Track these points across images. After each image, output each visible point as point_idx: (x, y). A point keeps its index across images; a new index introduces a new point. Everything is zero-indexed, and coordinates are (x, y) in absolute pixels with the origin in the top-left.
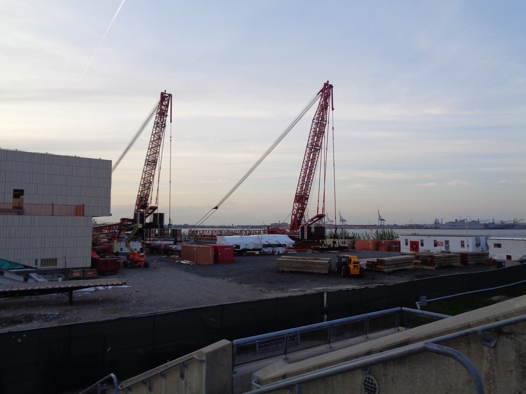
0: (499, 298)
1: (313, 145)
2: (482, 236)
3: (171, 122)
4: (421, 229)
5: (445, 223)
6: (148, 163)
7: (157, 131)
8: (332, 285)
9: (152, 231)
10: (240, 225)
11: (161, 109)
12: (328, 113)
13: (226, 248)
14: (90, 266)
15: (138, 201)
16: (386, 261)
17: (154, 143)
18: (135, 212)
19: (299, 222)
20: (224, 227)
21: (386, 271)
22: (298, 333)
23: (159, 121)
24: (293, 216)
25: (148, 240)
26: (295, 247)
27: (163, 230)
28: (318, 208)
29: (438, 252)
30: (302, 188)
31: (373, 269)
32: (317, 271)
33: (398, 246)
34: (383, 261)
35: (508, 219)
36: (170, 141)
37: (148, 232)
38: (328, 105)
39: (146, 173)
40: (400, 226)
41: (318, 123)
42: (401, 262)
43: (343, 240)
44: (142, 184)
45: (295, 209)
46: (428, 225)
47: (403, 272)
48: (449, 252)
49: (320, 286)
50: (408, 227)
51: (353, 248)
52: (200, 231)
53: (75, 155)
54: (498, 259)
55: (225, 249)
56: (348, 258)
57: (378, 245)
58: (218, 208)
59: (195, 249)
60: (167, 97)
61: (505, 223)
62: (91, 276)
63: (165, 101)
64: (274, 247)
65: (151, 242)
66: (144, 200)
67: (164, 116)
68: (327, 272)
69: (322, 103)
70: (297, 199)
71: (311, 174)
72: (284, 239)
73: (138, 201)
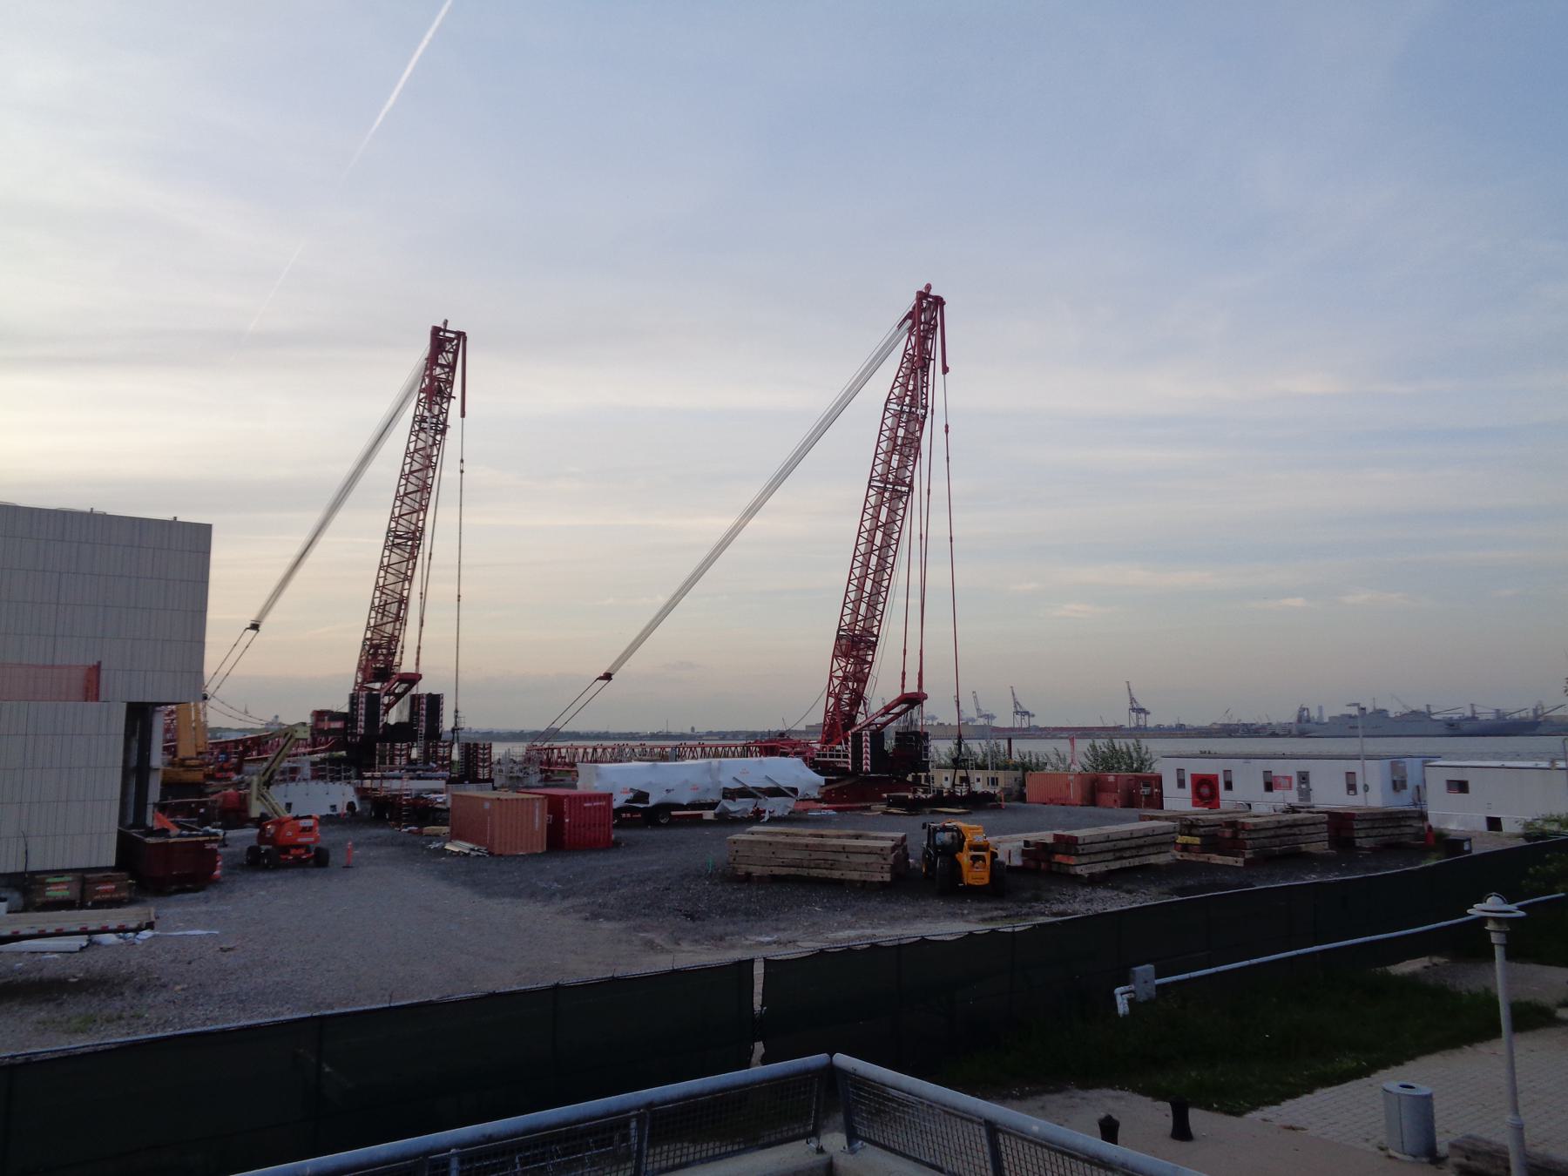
0: (1426, 964)
1: (886, 482)
2: (1411, 757)
3: (463, 415)
4: (1257, 737)
5: (1330, 718)
6: (393, 541)
7: (421, 444)
8: (893, 920)
9: (398, 750)
10: (715, 730)
11: (433, 378)
12: (931, 382)
13: (590, 802)
14: (112, 862)
15: (364, 658)
16: (1080, 842)
17: (412, 479)
18: (355, 690)
19: (851, 719)
20: (668, 736)
21: (1082, 873)
22: (632, 1113)
23: (426, 414)
24: (832, 700)
25: (368, 778)
26: (826, 798)
27: (433, 747)
28: (904, 674)
29: (1277, 809)
30: (856, 611)
31: (1043, 865)
32: (855, 876)
33: (1156, 790)
34: (1073, 841)
35: (1518, 705)
36: (459, 474)
37: (387, 753)
38: (930, 359)
39: (390, 570)
40: (1195, 729)
41: (902, 412)
42: (1133, 843)
43: (990, 773)
44: (376, 604)
45: (837, 677)
46: (1280, 724)
47: (1139, 876)
48: (1309, 811)
49: (850, 927)
50: (1217, 733)
51: (1022, 797)
52: (560, 749)
53: (92, 509)
54: (1461, 829)
55: (586, 805)
56: (959, 831)
57: (1093, 791)
58: (613, 677)
59: (487, 805)
60: (451, 340)
61: (1508, 718)
62: (108, 896)
63: (444, 354)
64: (760, 798)
65: (376, 784)
66: (382, 654)
67: (442, 398)
68: (887, 877)
69: (911, 352)
70: (841, 646)
71: (884, 570)
72: (792, 772)
73: (364, 658)
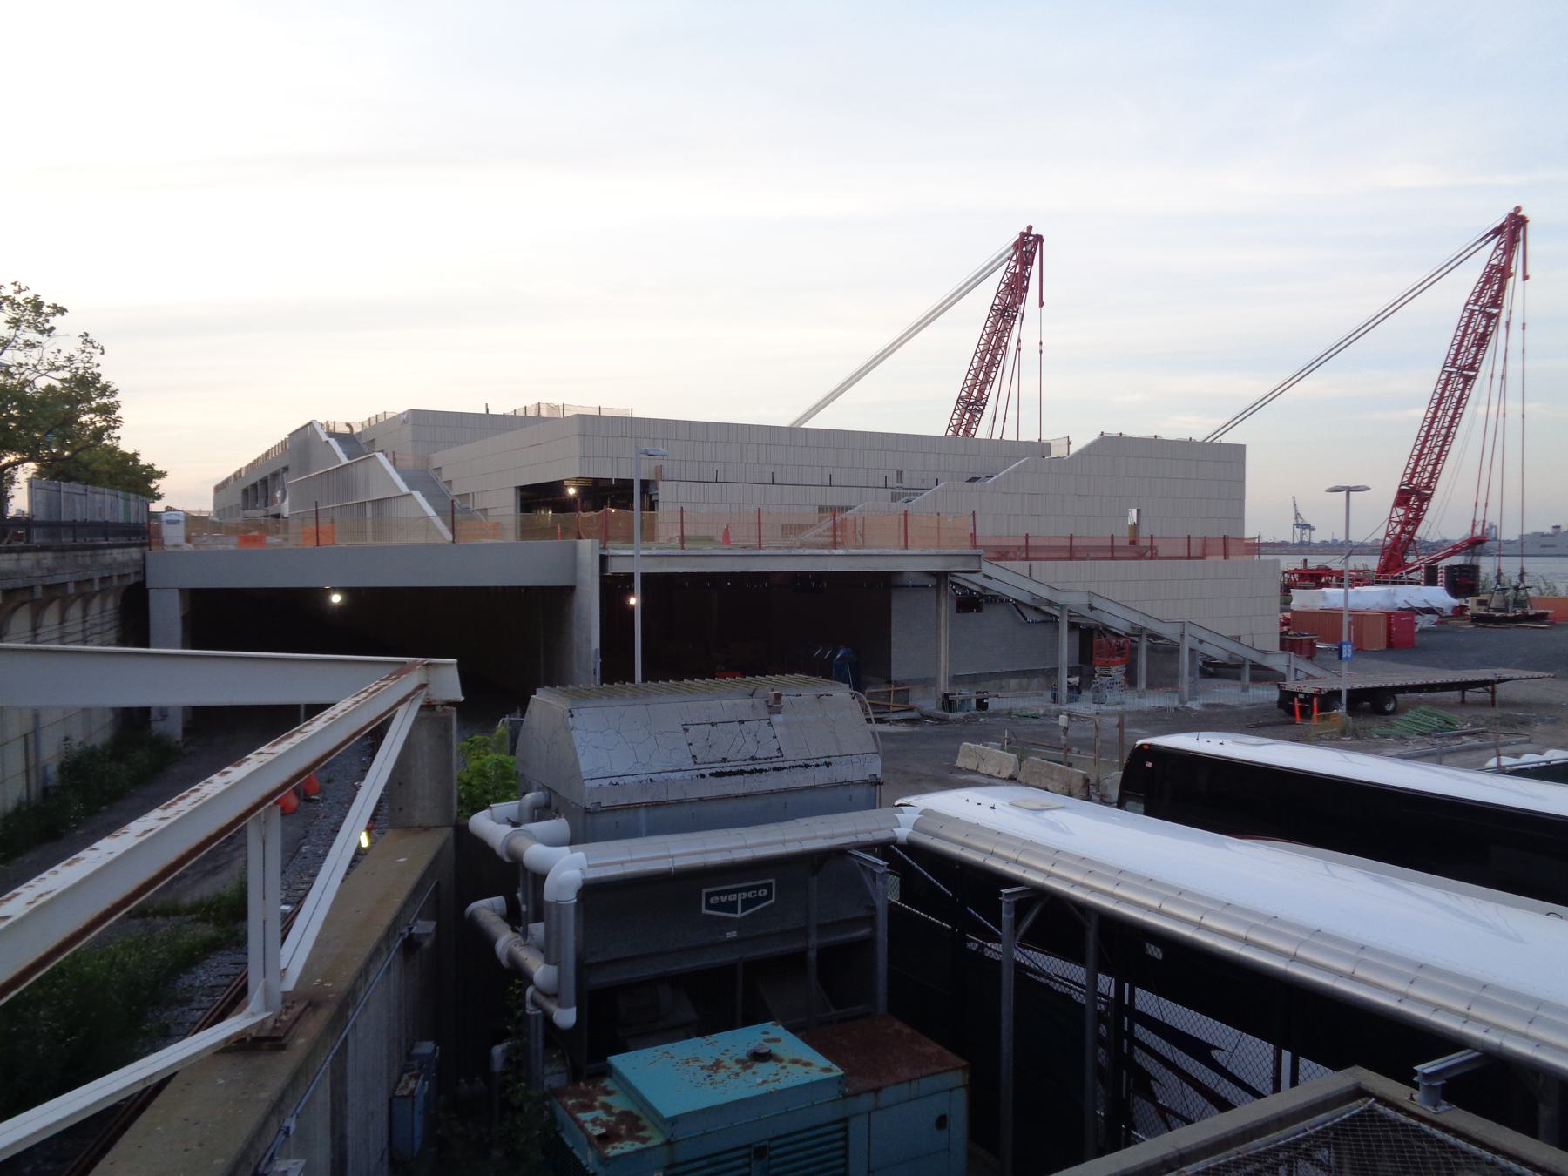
3: (1041, 304)
